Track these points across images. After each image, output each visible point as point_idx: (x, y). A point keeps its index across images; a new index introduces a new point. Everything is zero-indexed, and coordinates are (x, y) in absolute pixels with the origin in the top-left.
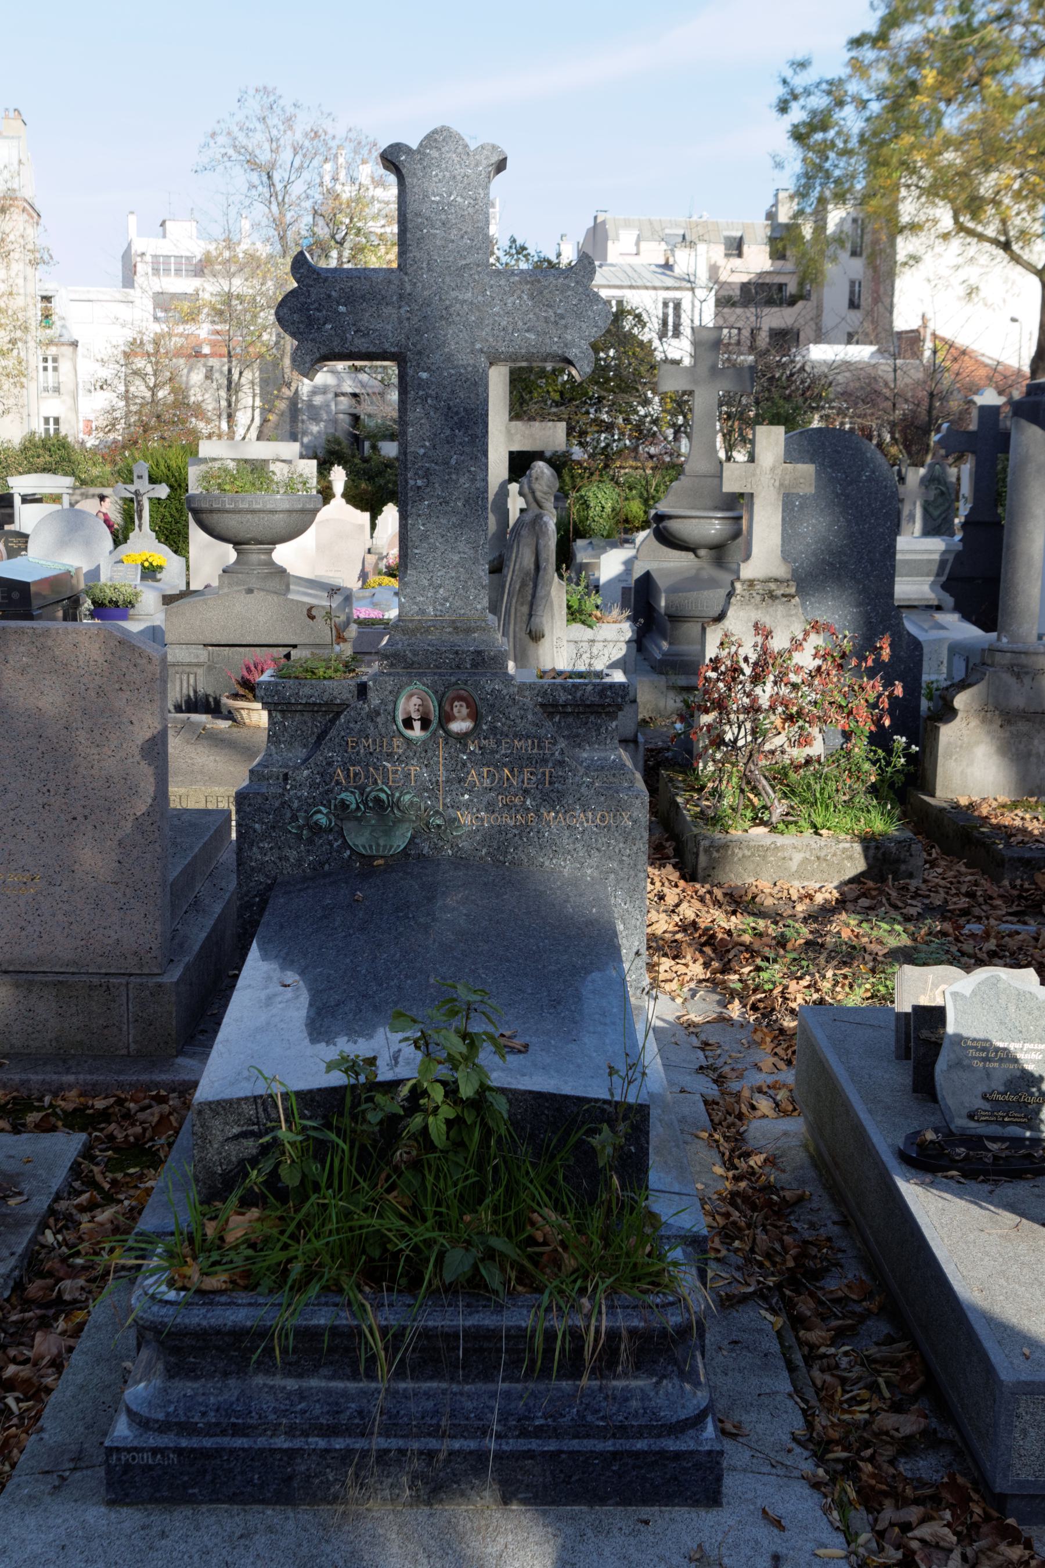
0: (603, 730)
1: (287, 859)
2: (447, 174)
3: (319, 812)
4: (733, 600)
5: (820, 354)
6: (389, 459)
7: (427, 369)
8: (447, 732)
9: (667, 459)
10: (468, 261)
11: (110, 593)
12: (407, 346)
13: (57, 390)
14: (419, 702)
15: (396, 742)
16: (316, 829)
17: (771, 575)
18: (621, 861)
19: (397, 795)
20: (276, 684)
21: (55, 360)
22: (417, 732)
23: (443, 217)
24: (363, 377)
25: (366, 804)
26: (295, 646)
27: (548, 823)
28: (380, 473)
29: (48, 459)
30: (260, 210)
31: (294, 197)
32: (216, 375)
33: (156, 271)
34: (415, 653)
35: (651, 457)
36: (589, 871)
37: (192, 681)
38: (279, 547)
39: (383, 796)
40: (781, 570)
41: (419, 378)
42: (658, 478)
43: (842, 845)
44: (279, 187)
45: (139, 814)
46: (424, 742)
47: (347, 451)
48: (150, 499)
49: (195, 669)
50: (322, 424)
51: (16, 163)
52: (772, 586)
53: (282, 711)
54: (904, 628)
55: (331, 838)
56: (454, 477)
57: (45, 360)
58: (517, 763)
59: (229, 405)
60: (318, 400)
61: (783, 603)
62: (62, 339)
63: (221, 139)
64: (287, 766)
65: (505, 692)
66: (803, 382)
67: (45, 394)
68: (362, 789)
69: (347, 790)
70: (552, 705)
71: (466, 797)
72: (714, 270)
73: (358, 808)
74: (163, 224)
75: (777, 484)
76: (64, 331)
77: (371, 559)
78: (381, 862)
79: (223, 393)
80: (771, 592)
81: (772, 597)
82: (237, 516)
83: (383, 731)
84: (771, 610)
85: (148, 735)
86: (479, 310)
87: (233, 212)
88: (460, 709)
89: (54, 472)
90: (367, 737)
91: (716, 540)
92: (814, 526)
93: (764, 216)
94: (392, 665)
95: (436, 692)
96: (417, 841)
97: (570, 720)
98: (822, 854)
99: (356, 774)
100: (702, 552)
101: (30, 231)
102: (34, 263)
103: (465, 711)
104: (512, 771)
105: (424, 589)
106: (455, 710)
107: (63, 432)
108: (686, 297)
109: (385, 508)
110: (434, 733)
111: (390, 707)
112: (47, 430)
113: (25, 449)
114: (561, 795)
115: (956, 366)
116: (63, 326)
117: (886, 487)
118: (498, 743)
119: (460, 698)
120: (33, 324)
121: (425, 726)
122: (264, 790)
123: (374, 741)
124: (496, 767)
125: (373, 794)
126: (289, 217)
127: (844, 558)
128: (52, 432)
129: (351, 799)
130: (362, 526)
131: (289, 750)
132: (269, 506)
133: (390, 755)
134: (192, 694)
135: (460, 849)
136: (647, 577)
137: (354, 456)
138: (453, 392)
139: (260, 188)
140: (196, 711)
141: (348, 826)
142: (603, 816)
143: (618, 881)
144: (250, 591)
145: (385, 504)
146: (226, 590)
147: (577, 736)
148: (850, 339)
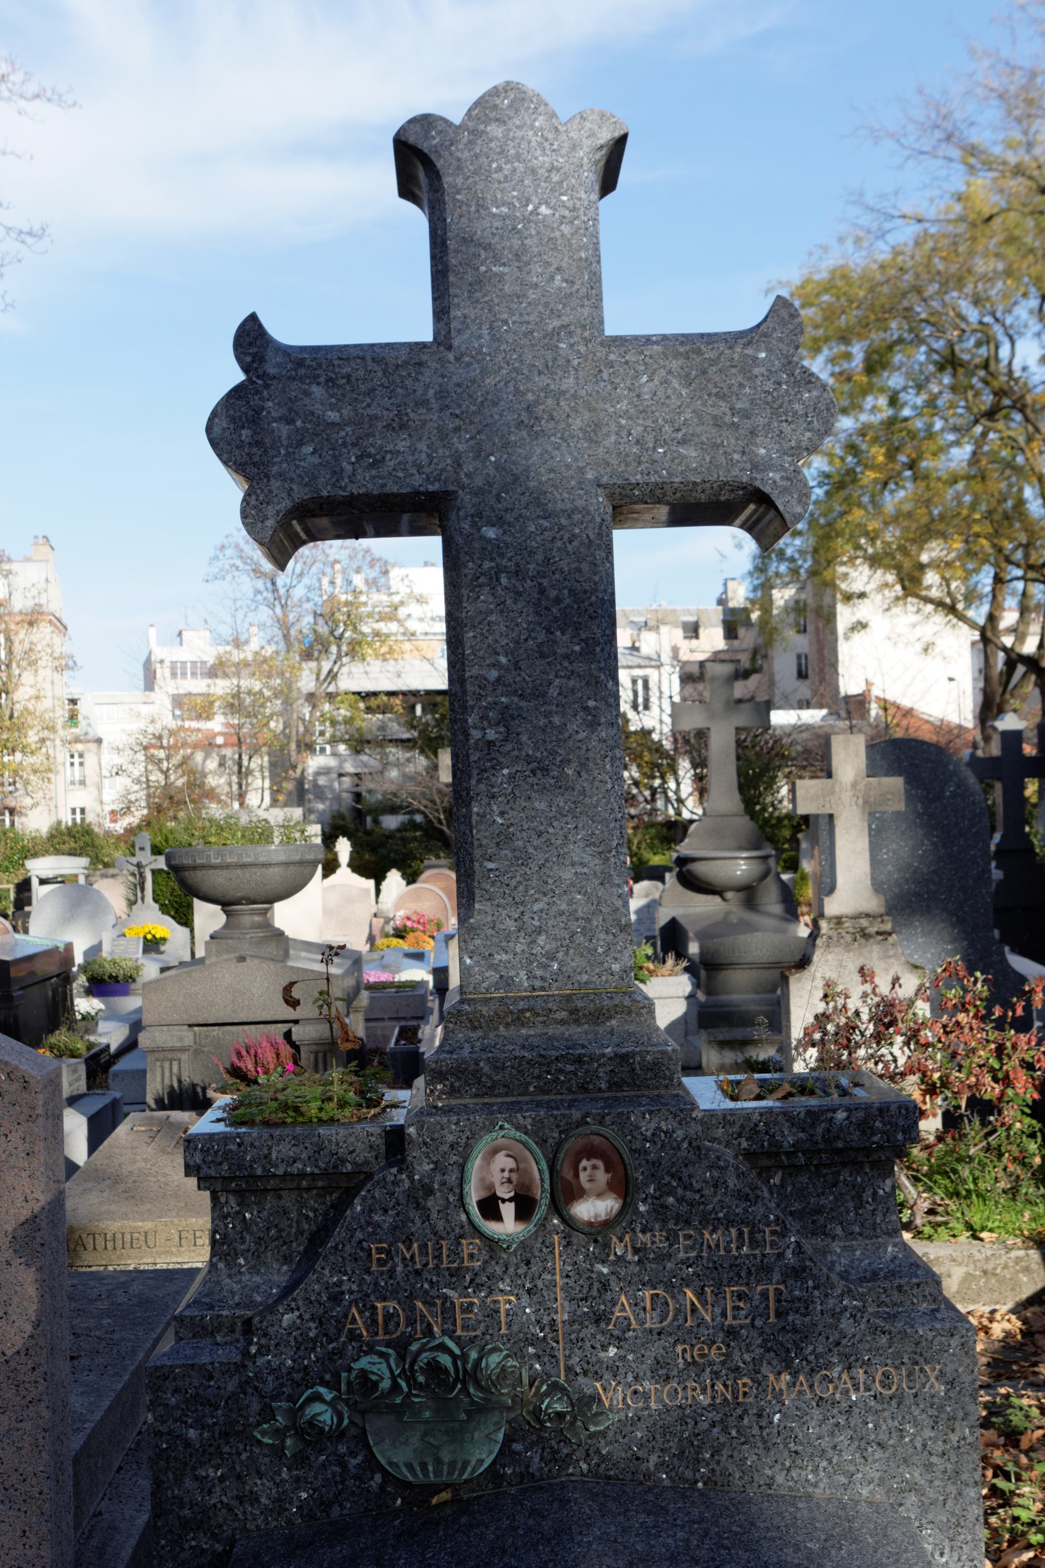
0: (867, 1196)
1: (254, 1498)
2: (520, 167)
3: (317, 1398)
4: (819, 942)
5: (781, 718)
6: (391, 831)
7: (498, 521)
8: (568, 1221)
9: (646, 818)
10: (565, 320)
11: (109, 969)
12: (458, 481)
13: (83, 783)
14: (510, 1163)
15: (468, 1247)
16: (312, 1435)
17: (861, 910)
18: (928, 1467)
19: (474, 1355)
20: (225, 1138)
21: (81, 756)
22: (508, 1226)
23: (516, 243)
24: (364, 758)
25: (411, 1380)
26: (296, 1022)
27: (778, 1395)
28: (382, 845)
29: (73, 845)
30: (264, 614)
31: (296, 599)
32: (229, 763)
33: (174, 675)
34: (498, 1066)
35: (632, 817)
36: (865, 1492)
37: (175, 1069)
38: (278, 906)
39: (445, 1360)
40: (872, 903)
41: (482, 538)
42: (639, 836)
43: (1014, 1254)
44: (282, 591)
45: (9, 1353)
46: (523, 1245)
47: (352, 826)
48: (153, 872)
49: (179, 1055)
50: (328, 803)
51: (43, 580)
52: (864, 922)
53: (239, 1192)
54: (1009, 966)
55: (342, 1449)
56: (556, 720)
57: (72, 756)
58: (716, 1274)
59: (240, 787)
60: (322, 781)
61: (879, 943)
62: (89, 737)
63: (229, 552)
64: (251, 1304)
65: (680, 1134)
66: (767, 743)
67: (72, 787)
68: (401, 1346)
69: (371, 1351)
70: (769, 1155)
71: (612, 1351)
72: (675, 650)
73: (395, 1387)
74: (180, 634)
75: (860, 802)
76: (90, 730)
77: (378, 923)
78: (445, 1496)
79: (235, 779)
80: (862, 930)
81: (865, 935)
82: (224, 873)
83: (440, 1225)
84: (864, 951)
85: (25, 1213)
86: (591, 409)
87: (240, 614)
88: (593, 1173)
89: (80, 855)
90: (408, 1242)
91: (744, 881)
92: (894, 852)
93: (715, 602)
94: (453, 1092)
95: (542, 1143)
96: (517, 1447)
97: (804, 1179)
98: (989, 1267)
99: (388, 1317)
100: (729, 895)
101: (57, 640)
102: (59, 669)
103: (602, 1177)
104: (700, 1294)
105: (507, 938)
106: (583, 1177)
107: (88, 821)
108: (653, 674)
109: (389, 874)
110: (542, 1225)
111: (452, 1178)
112: (74, 820)
113: (51, 837)
114: (802, 1335)
115: (904, 723)
116: (89, 725)
117: (974, 803)
118: (672, 1238)
119: (590, 1152)
120: (60, 722)
121: (524, 1211)
122: (205, 1359)
123: (423, 1247)
124: (669, 1287)
125: (425, 1356)
126: (291, 617)
127: (932, 887)
128: (78, 821)
129: (379, 1367)
130: (367, 890)
131: (254, 1270)
132: (262, 859)
133: (456, 1273)
134: (176, 1085)
135: (603, 1459)
136: (673, 923)
137: (357, 830)
138: (547, 560)
139: (265, 594)
140: (172, 1107)
141: (374, 1425)
142: (886, 1375)
143: (924, 1508)
144: (242, 959)
145: (388, 870)
146: (214, 959)
147: (819, 1211)
148: (805, 704)
